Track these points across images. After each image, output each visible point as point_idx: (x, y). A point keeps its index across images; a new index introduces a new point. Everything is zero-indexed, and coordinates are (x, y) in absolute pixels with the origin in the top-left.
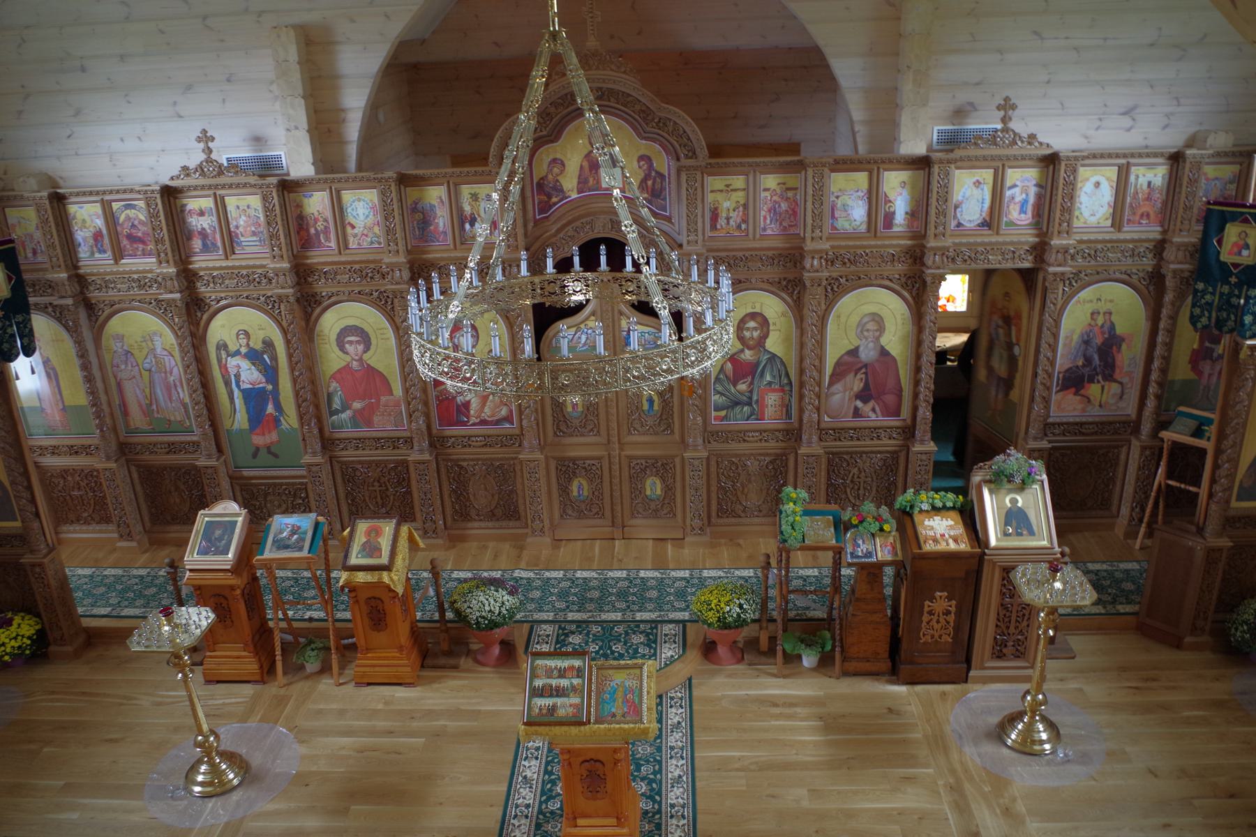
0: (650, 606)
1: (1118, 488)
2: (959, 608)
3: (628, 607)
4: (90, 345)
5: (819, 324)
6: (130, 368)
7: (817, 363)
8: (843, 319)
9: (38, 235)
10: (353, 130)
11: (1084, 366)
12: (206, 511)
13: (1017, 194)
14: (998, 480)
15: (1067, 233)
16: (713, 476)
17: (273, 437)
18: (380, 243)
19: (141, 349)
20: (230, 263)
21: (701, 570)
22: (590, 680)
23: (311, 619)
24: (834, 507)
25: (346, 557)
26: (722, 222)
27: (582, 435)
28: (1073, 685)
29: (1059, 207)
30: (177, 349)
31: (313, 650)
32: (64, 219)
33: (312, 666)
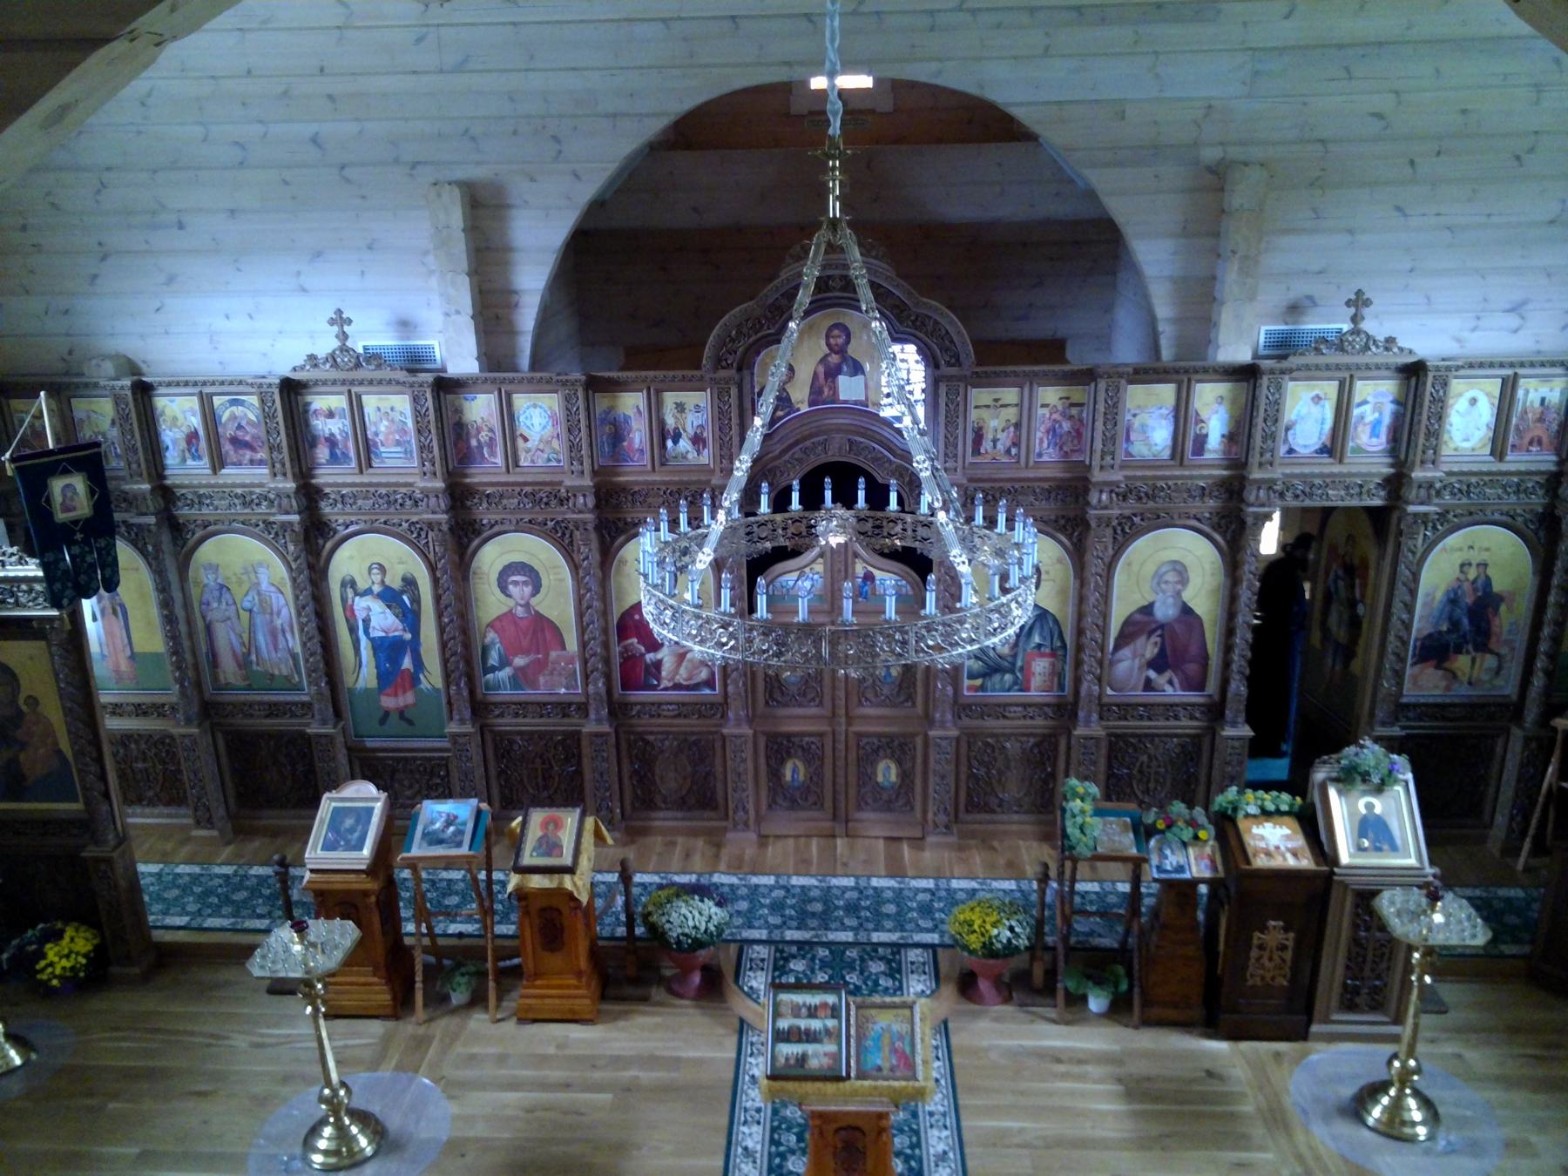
0: (888, 924)
1: (1491, 791)
2: (1298, 943)
3: (861, 925)
4: (173, 576)
5: (1104, 574)
6: (224, 606)
7: (1100, 623)
8: (1135, 568)
9: (114, 433)
10: (527, 318)
11: (1449, 631)
12: (334, 794)
13: (1368, 412)
14: (1349, 778)
15: (1433, 463)
16: (964, 760)
17: (408, 698)
18: (559, 461)
19: (240, 583)
20: (365, 479)
21: (949, 879)
22: (848, 1020)
23: (461, 935)
24: (1132, 806)
25: (518, 855)
26: (987, 445)
27: (800, 705)
28: (1449, 1049)
29: (1423, 430)
30: (289, 584)
31: (463, 975)
32: (149, 413)
33: (458, 997)
